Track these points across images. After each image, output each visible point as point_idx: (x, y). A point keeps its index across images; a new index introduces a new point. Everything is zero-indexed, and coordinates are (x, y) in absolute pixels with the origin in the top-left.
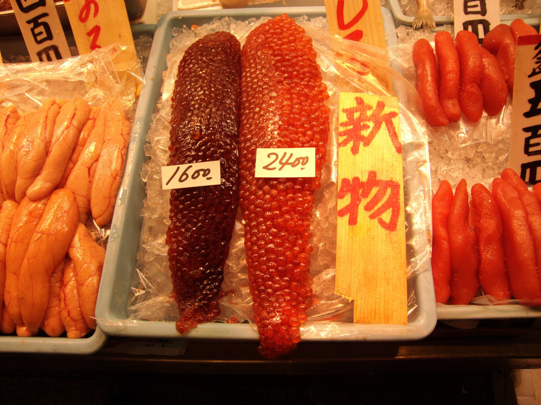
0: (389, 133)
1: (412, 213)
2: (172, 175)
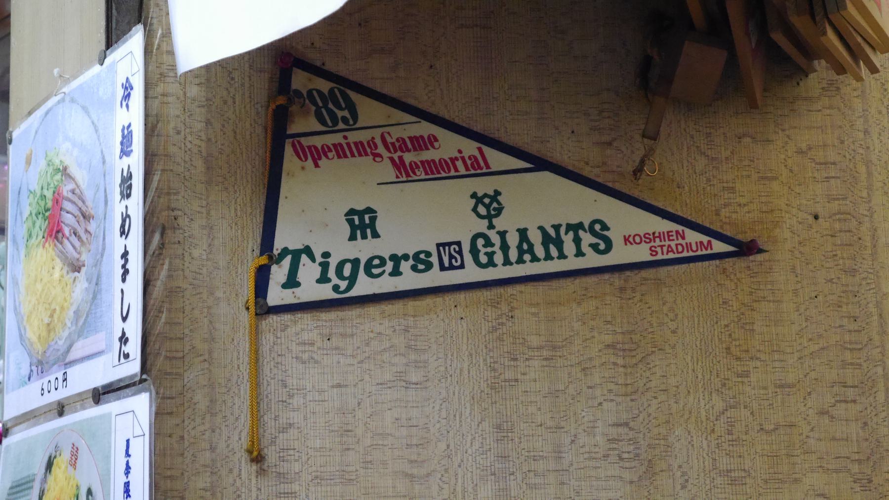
0: (131, 184)
1: (758, 108)
2: (375, 129)
